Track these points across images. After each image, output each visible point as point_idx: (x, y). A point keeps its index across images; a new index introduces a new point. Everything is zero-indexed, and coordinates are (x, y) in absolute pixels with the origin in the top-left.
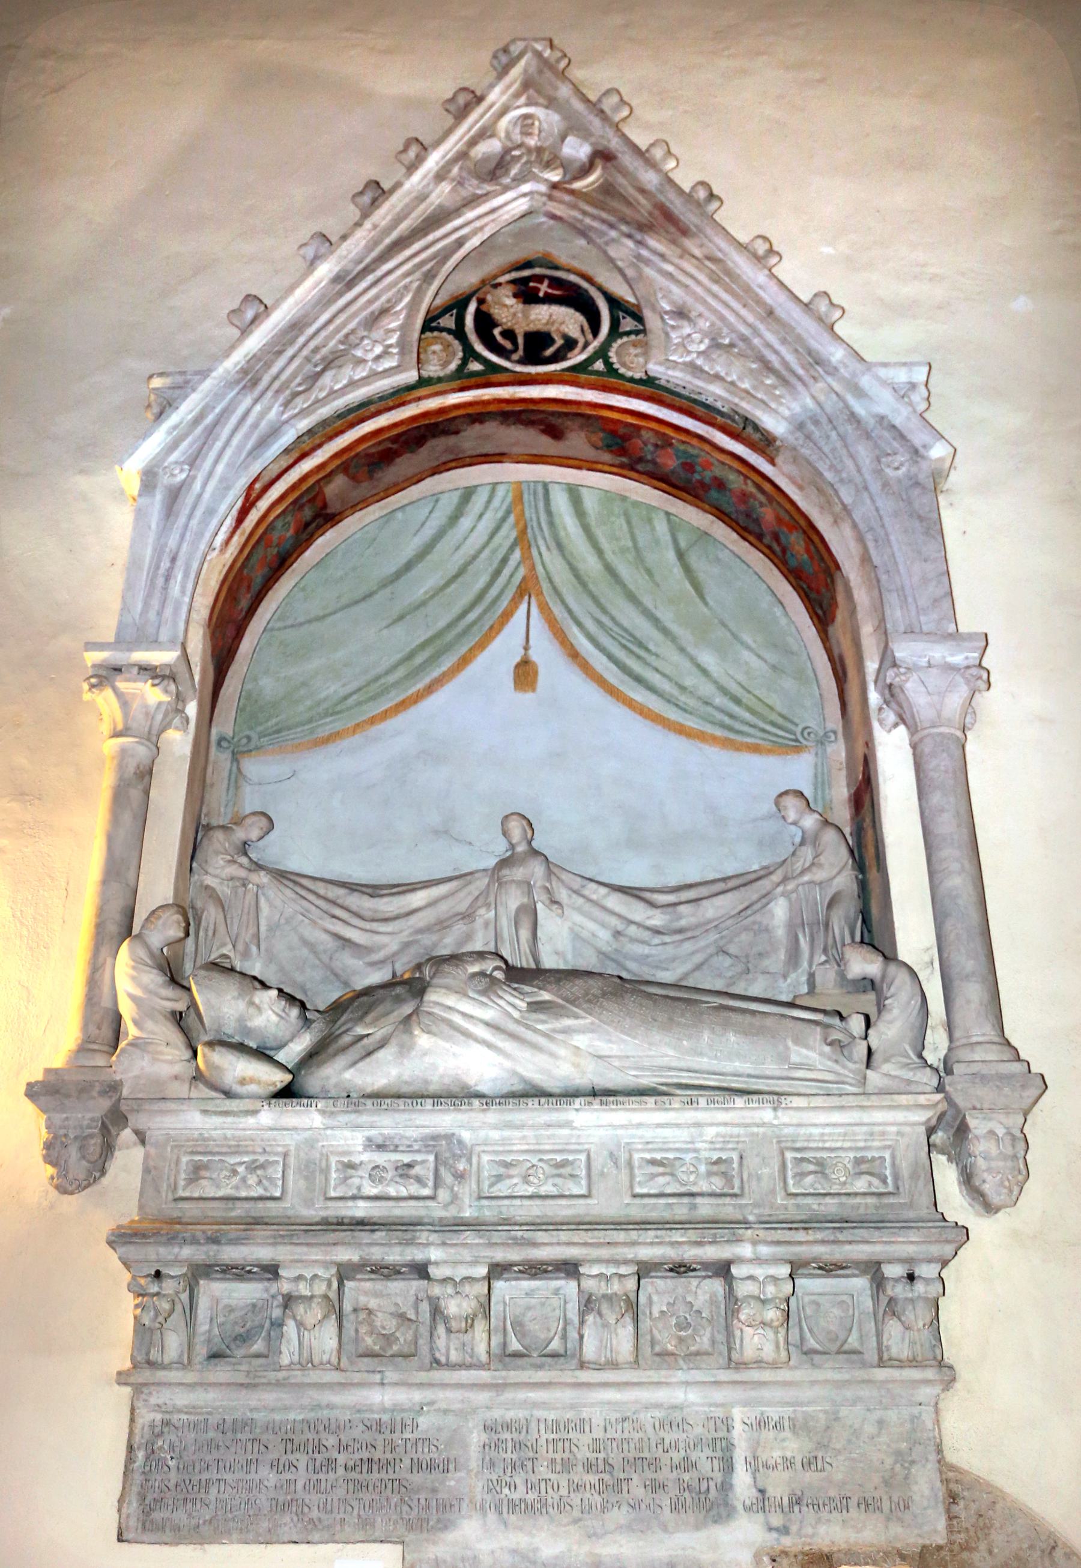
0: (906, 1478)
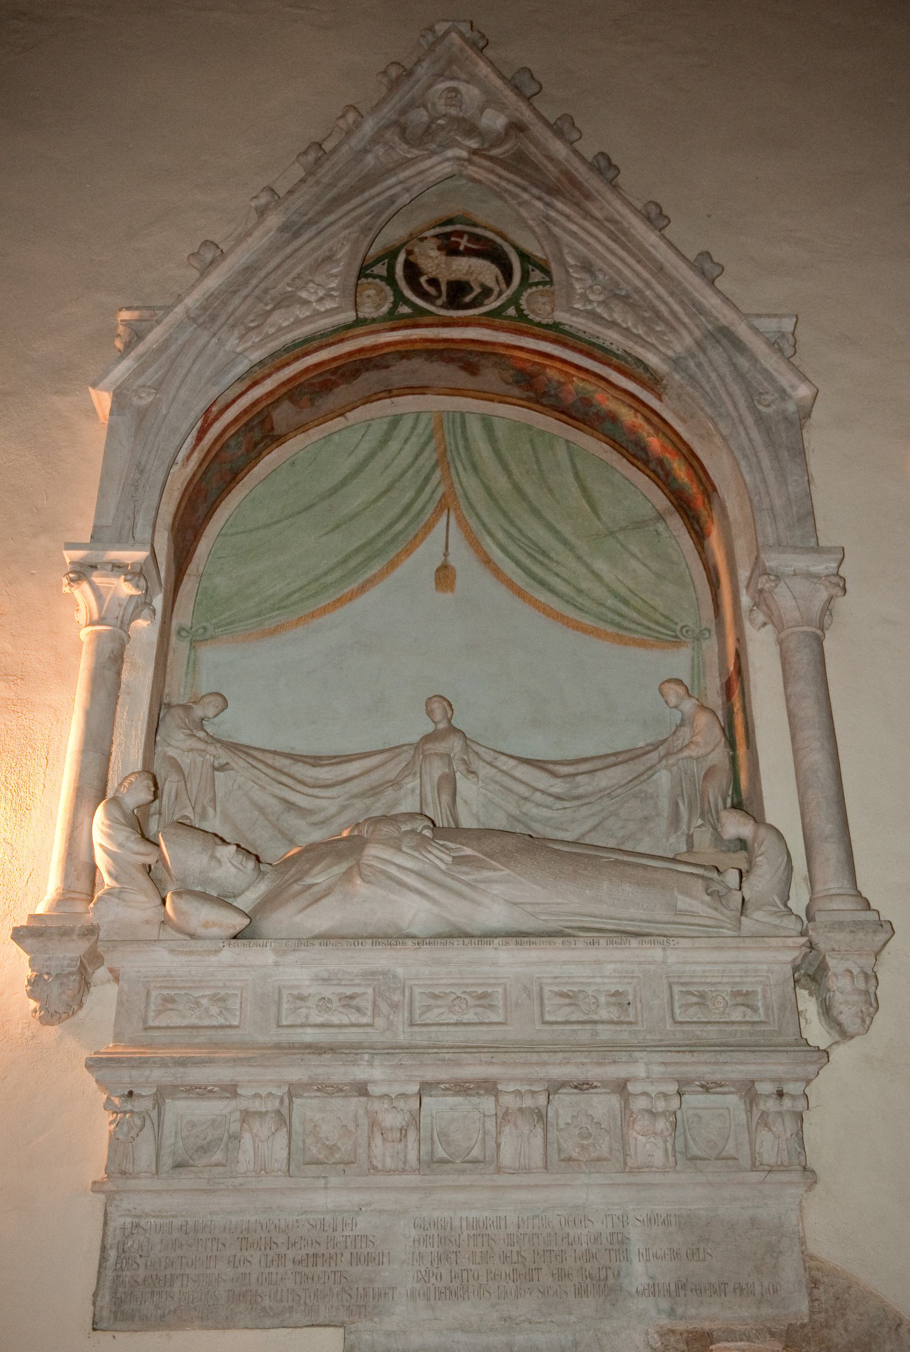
0: (775, 1267)
